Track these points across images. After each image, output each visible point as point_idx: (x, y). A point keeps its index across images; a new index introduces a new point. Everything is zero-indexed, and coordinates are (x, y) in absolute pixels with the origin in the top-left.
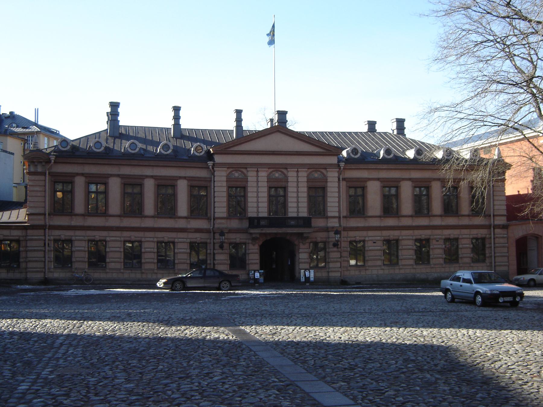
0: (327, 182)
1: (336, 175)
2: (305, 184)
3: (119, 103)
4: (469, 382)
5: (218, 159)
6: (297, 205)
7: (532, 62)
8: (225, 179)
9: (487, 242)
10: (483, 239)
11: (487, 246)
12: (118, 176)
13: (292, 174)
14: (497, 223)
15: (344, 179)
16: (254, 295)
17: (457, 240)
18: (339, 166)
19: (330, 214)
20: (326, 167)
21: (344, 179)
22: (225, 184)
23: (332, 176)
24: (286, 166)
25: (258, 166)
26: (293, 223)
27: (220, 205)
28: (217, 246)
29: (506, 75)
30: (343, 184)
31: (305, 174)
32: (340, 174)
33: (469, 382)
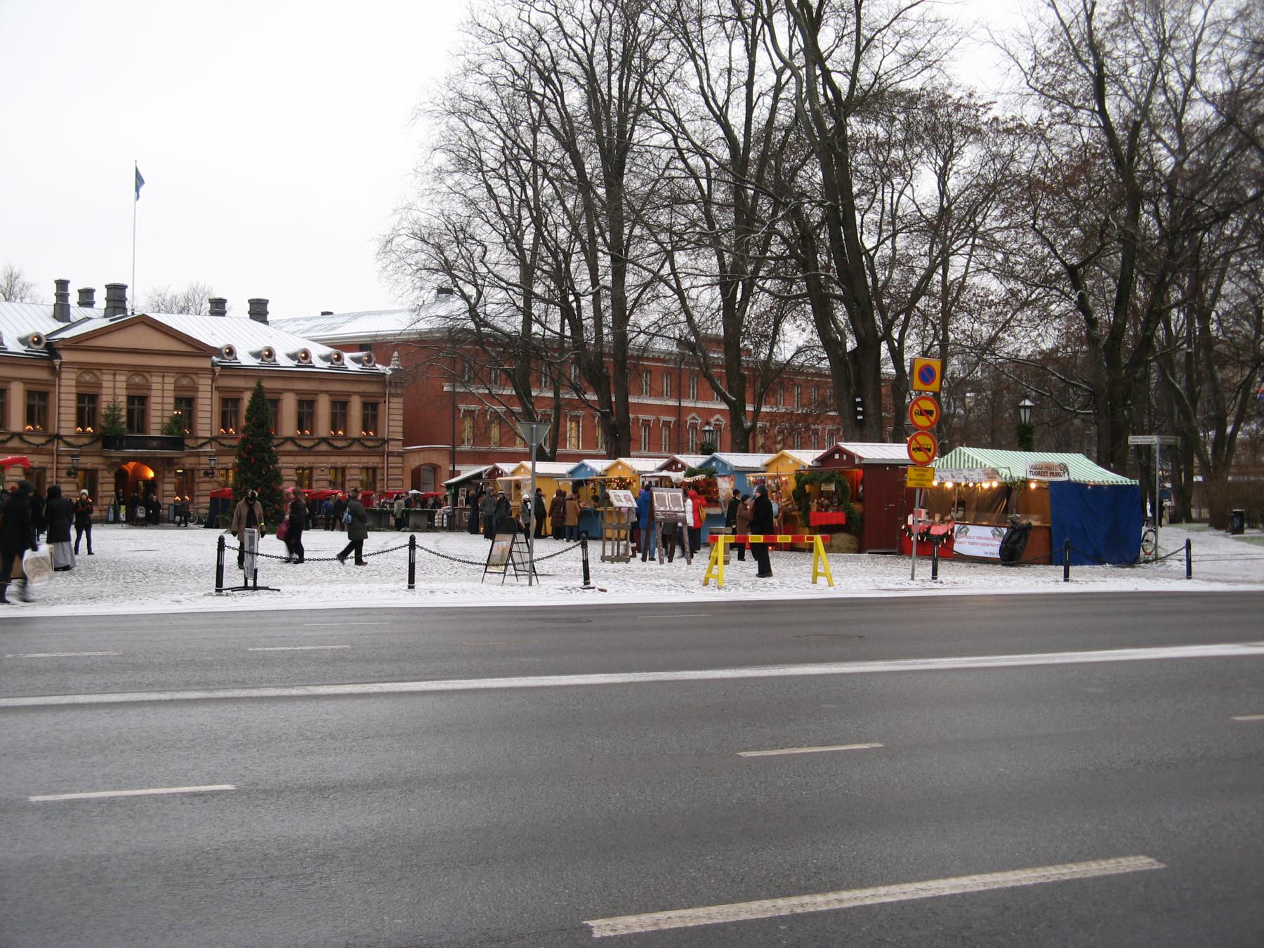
0: (150, 389)
1: (209, 382)
2: (172, 394)
3: (250, 301)
4: (1071, 182)
5: (66, 356)
6: (161, 411)
7: (557, 19)
8: (74, 383)
9: (379, 472)
10: (374, 469)
11: (379, 477)
12: (21, 379)
13: (156, 381)
14: (391, 449)
15: (217, 388)
16: (127, 797)
17: (343, 469)
18: (213, 371)
19: (200, 434)
20: (197, 371)
21: (217, 388)
22: (74, 390)
23: (204, 384)
24: (149, 369)
25: (115, 368)
26: (155, 443)
27: (65, 418)
28: (64, 473)
29: (534, 13)
30: (216, 395)
31: (172, 380)
32: (213, 381)
33: (1071, 182)
